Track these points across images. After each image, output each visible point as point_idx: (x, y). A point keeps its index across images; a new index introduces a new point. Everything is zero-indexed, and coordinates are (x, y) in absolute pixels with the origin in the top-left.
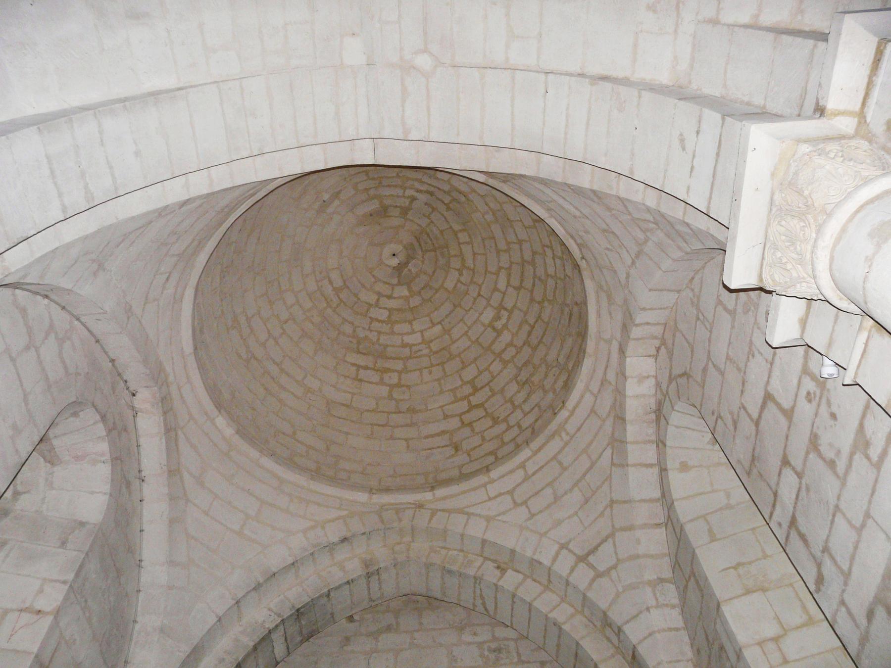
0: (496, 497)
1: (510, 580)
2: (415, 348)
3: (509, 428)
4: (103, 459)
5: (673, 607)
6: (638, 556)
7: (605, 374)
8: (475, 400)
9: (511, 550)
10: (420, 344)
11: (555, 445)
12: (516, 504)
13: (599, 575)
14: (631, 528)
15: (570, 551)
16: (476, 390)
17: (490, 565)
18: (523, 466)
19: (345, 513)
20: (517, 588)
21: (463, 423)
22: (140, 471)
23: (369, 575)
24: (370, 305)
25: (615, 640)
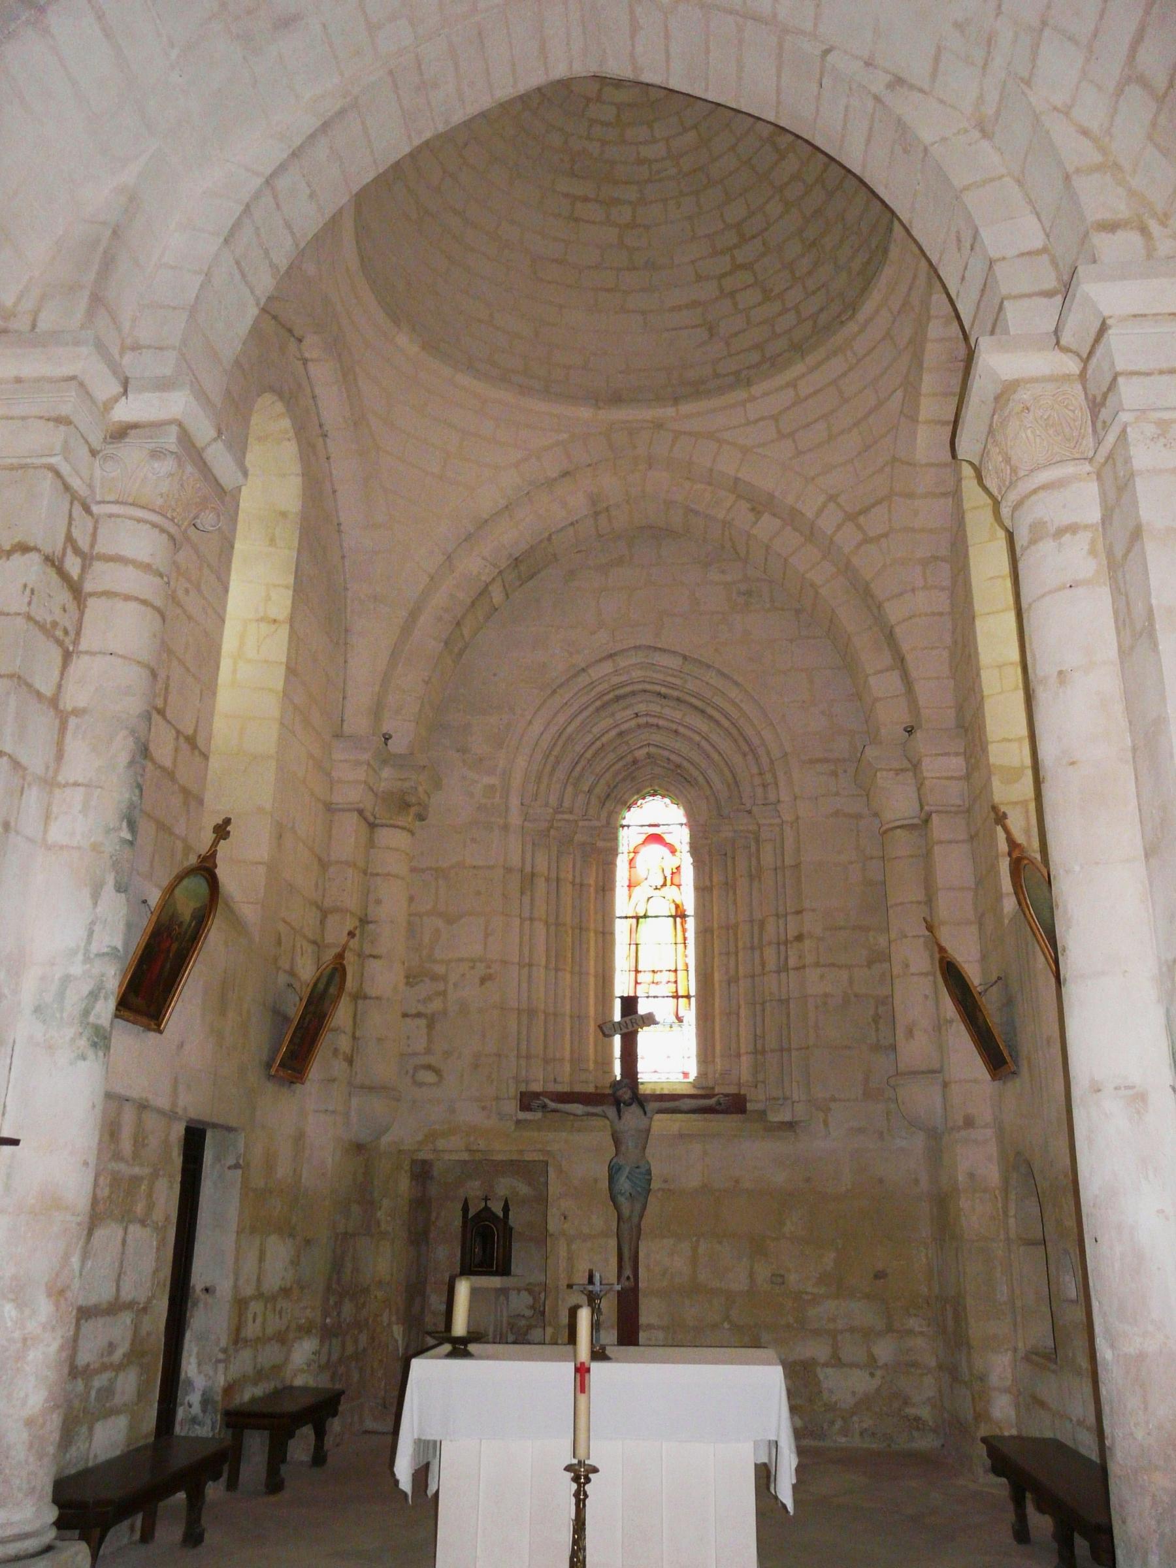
0: (756, 421)
1: (767, 525)
2: (655, 167)
3: (785, 311)
4: (287, 436)
5: (943, 589)
6: (913, 530)
7: (908, 295)
8: (741, 256)
9: (769, 494)
10: (663, 159)
11: (837, 365)
12: (782, 436)
13: (867, 541)
14: (911, 495)
15: (838, 505)
16: (744, 239)
17: (744, 505)
18: (793, 384)
19: (565, 436)
20: (771, 539)
21: (721, 290)
22: (321, 426)
23: (596, 514)
24: (588, 100)
25: (875, 611)
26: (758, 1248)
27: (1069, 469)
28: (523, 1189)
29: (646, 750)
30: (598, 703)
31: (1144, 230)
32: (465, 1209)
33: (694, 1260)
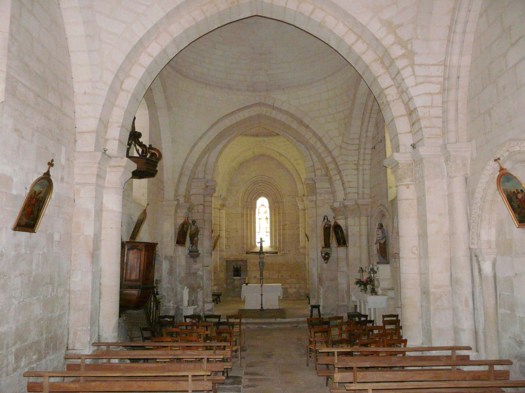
13: (298, 164)
26: (279, 272)
28: (242, 264)
31: (322, 170)
32: (234, 267)
33: (270, 274)
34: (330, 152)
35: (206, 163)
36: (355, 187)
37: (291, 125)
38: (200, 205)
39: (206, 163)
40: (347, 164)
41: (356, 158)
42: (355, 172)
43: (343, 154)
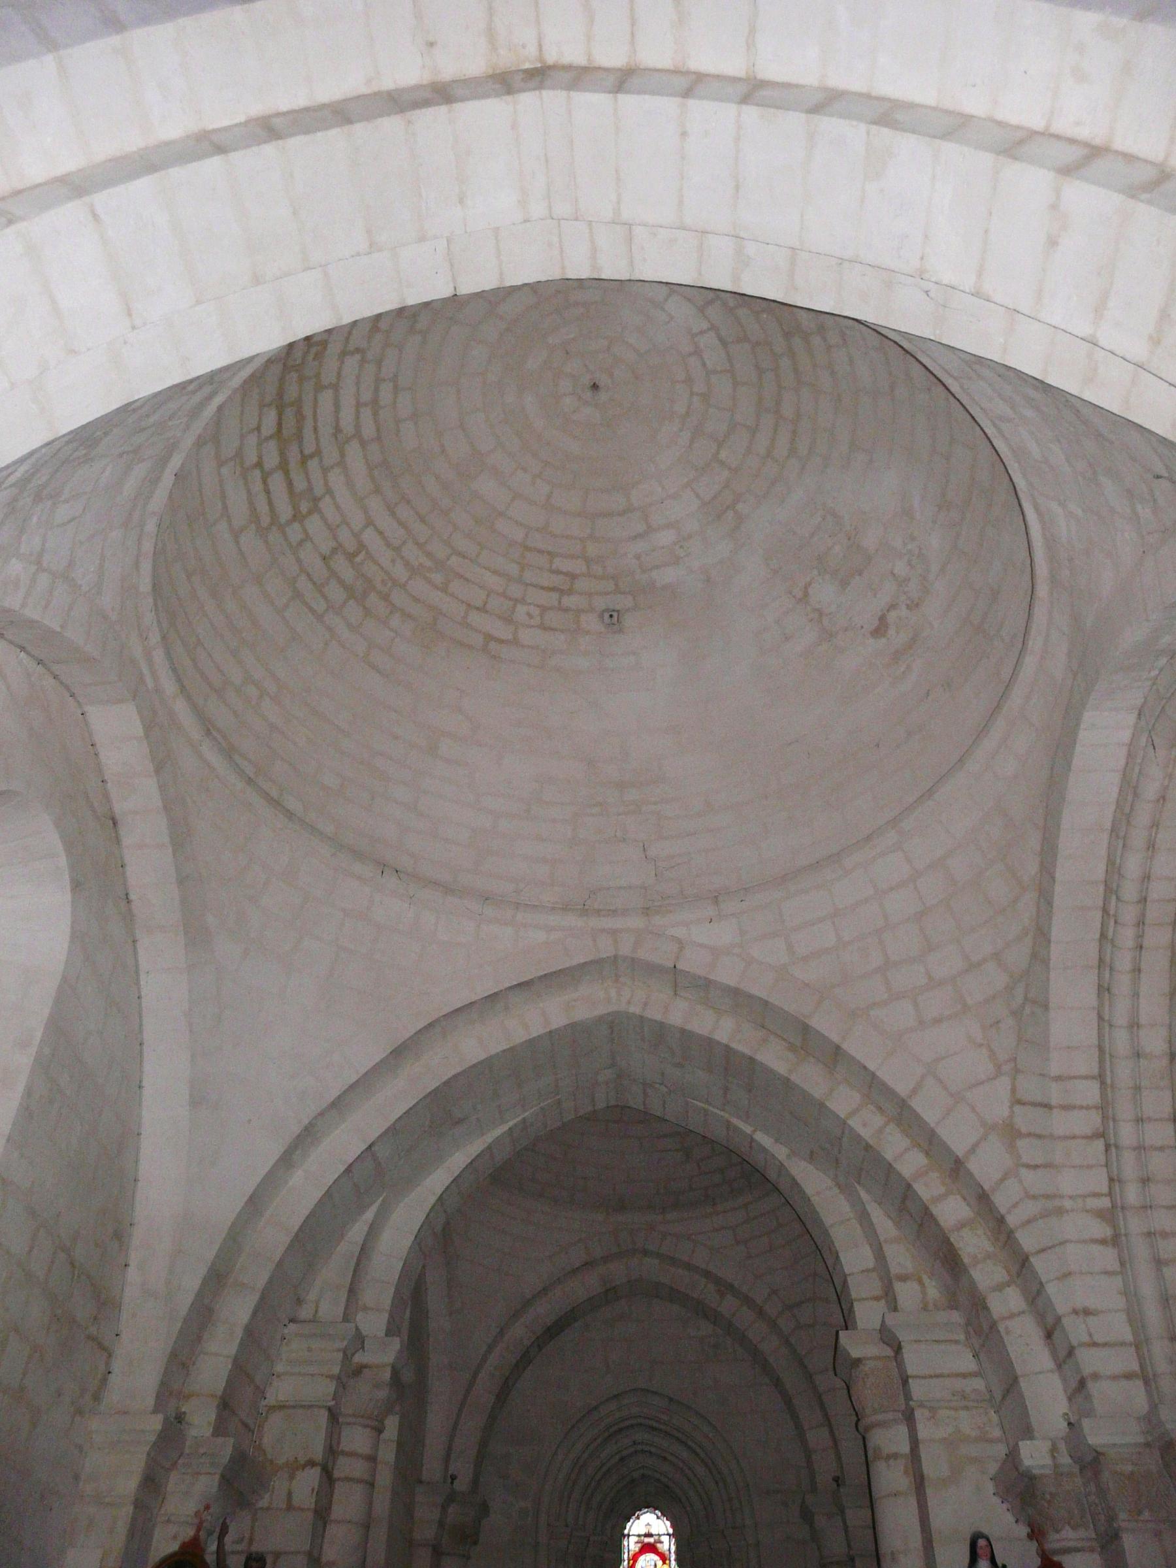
27: (890, 1416)
29: (642, 1471)
30: (606, 1434)
31: (920, 1282)
34: (956, 1169)
35: (365, 1251)
36: (1123, 1344)
37: (759, 1057)
38: (304, 1467)
39: (365, 1251)
40: (1060, 1212)
41: (1098, 1181)
42: (1108, 1257)
43: (1028, 1166)
